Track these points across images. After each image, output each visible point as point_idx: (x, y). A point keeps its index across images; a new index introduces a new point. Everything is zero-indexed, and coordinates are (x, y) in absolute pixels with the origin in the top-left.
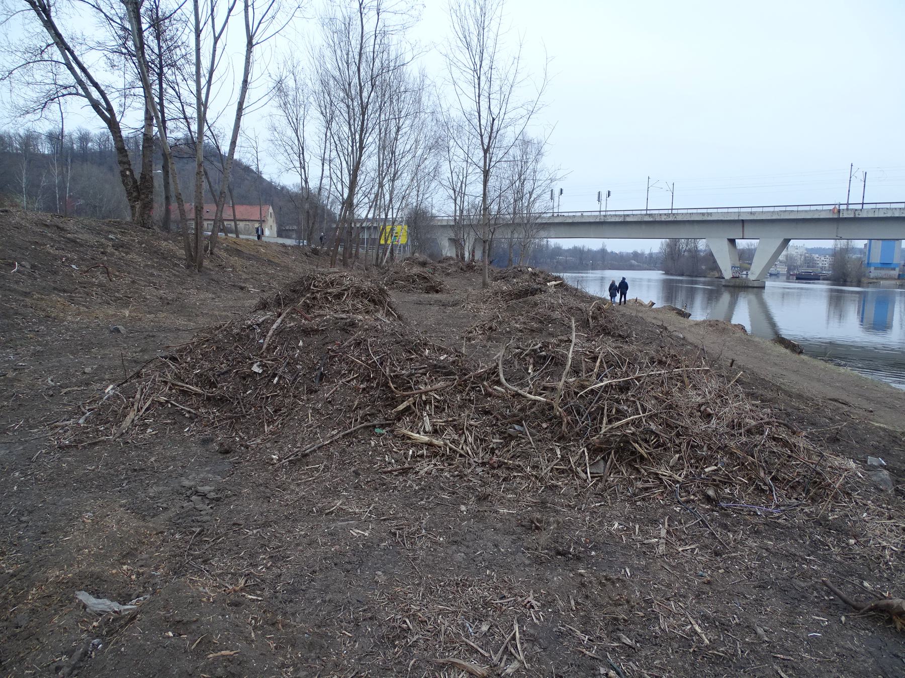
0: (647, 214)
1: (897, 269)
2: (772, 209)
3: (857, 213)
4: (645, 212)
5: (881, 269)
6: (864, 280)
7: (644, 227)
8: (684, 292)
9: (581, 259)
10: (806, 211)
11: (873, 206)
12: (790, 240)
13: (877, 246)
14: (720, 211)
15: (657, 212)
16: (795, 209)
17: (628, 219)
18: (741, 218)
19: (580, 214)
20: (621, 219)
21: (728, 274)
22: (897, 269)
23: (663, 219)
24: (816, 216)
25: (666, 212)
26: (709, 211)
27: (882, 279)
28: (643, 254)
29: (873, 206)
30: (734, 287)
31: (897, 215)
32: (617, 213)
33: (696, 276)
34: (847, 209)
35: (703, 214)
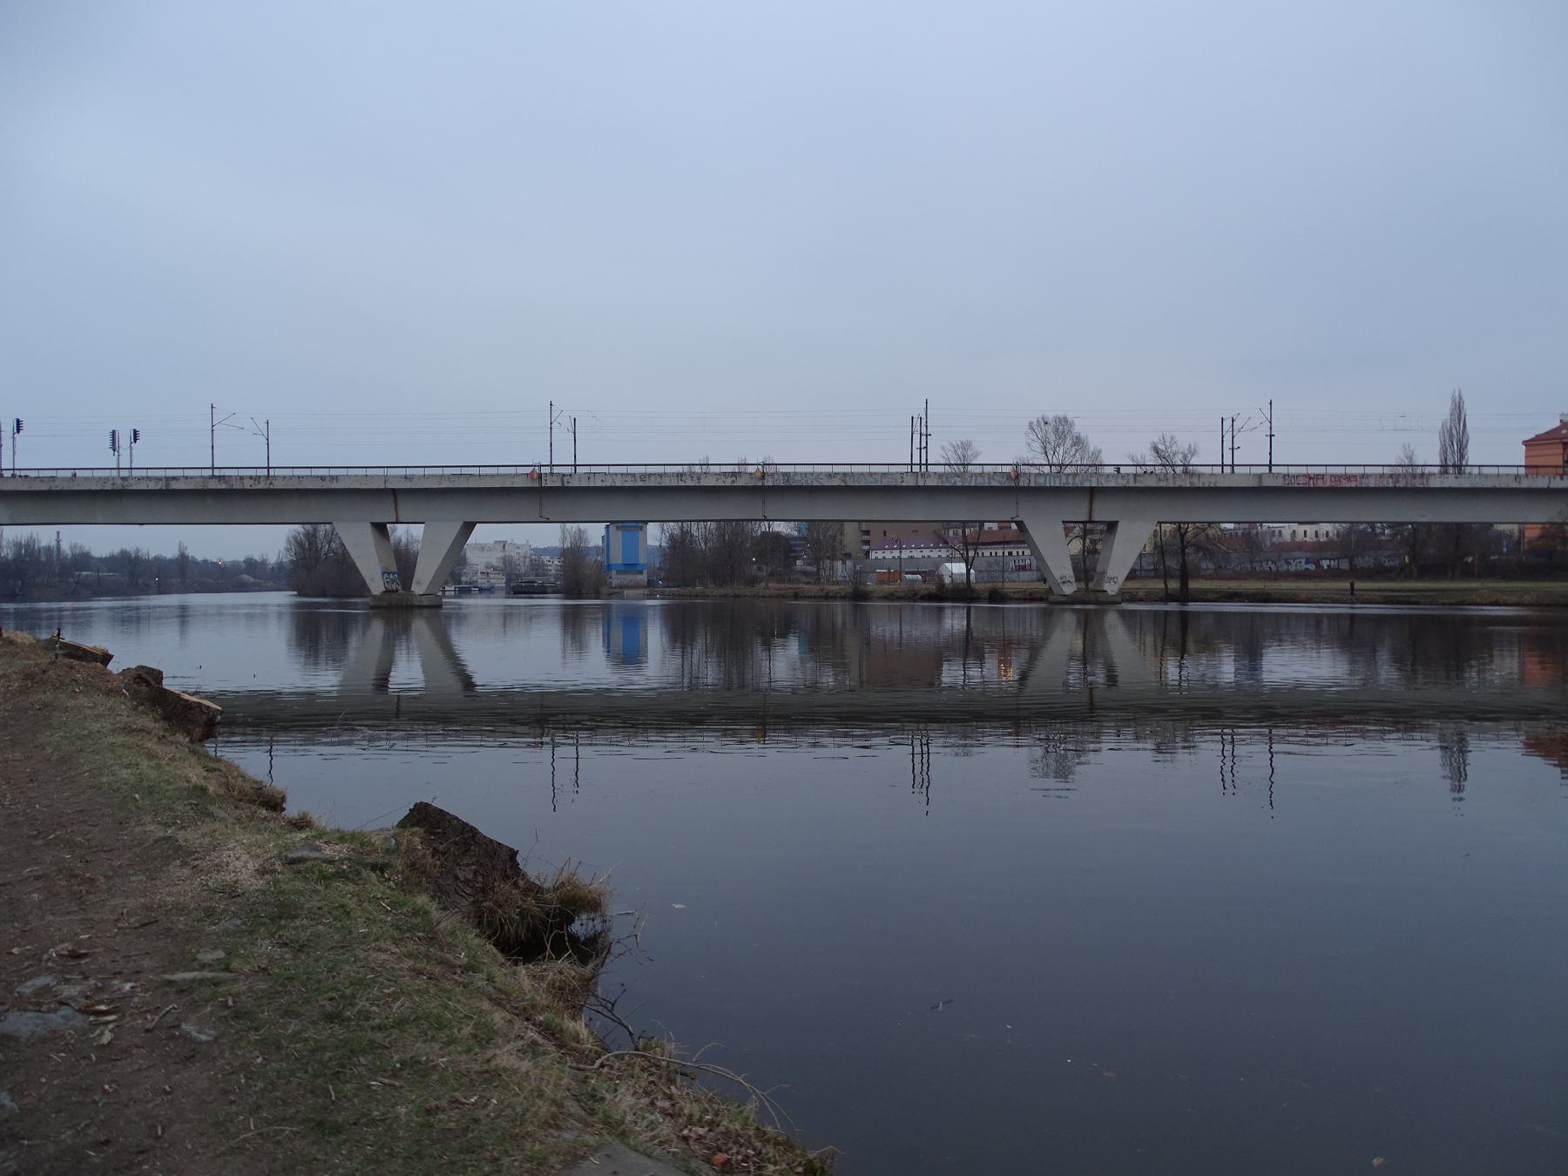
0: (213, 477)
2: (439, 471)
4: (209, 472)
5: (625, 572)
6: (604, 590)
10: (492, 476)
12: (474, 524)
13: (617, 536)
14: (351, 472)
15: (234, 473)
16: (475, 471)
17: (175, 485)
19: (69, 474)
21: (377, 586)
23: (247, 487)
24: (508, 485)
26: (334, 472)
27: (627, 587)
28: (263, 563)
30: (389, 608)
31: (618, 484)
32: (151, 473)
33: (348, 597)
35: (322, 478)
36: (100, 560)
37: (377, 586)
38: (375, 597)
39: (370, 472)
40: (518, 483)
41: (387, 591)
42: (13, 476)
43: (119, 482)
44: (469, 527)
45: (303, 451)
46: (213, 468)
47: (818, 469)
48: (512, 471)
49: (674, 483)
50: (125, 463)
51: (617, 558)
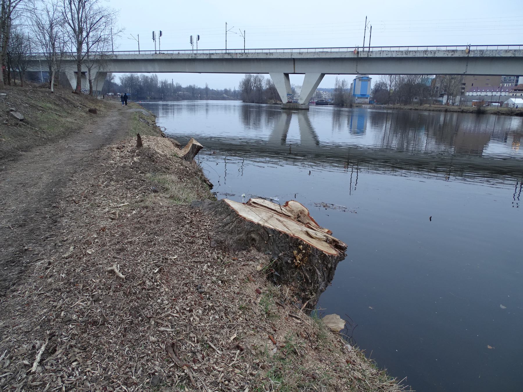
0: (226, 53)
1: (369, 98)
2: (313, 50)
3: (369, 54)
4: (224, 52)
5: (361, 98)
7: (224, 63)
8: (254, 114)
9: (193, 93)
10: (337, 52)
11: (380, 49)
14: (131, 53)
15: (233, 51)
16: (329, 50)
17: (213, 57)
18: (293, 57)
19: (177, 52)
20: (207, 57)
22: (369, 98)
23: (238, 57)
24: (343, 56)
25: (240, 51)
28: (230, 91)
29: (380, 49)
30: (290, 109)
31: (394, 56)
33: (261, 103)
34: (363, 51)
35: (267, 54)
36: (184, 88)
37: (285, 100)
38: (284, 104)
39: (286, 51)
40: (348, 56)
41: (289, 102)
42: (160, 53)
43: (194, 55)
44: (323, 75)
45: (259, 42)
46: (226, 50)
47: (500, 48)
48: (345, 50)
49: (422, 55)
50: (195, 48)
51: (358, 92)
